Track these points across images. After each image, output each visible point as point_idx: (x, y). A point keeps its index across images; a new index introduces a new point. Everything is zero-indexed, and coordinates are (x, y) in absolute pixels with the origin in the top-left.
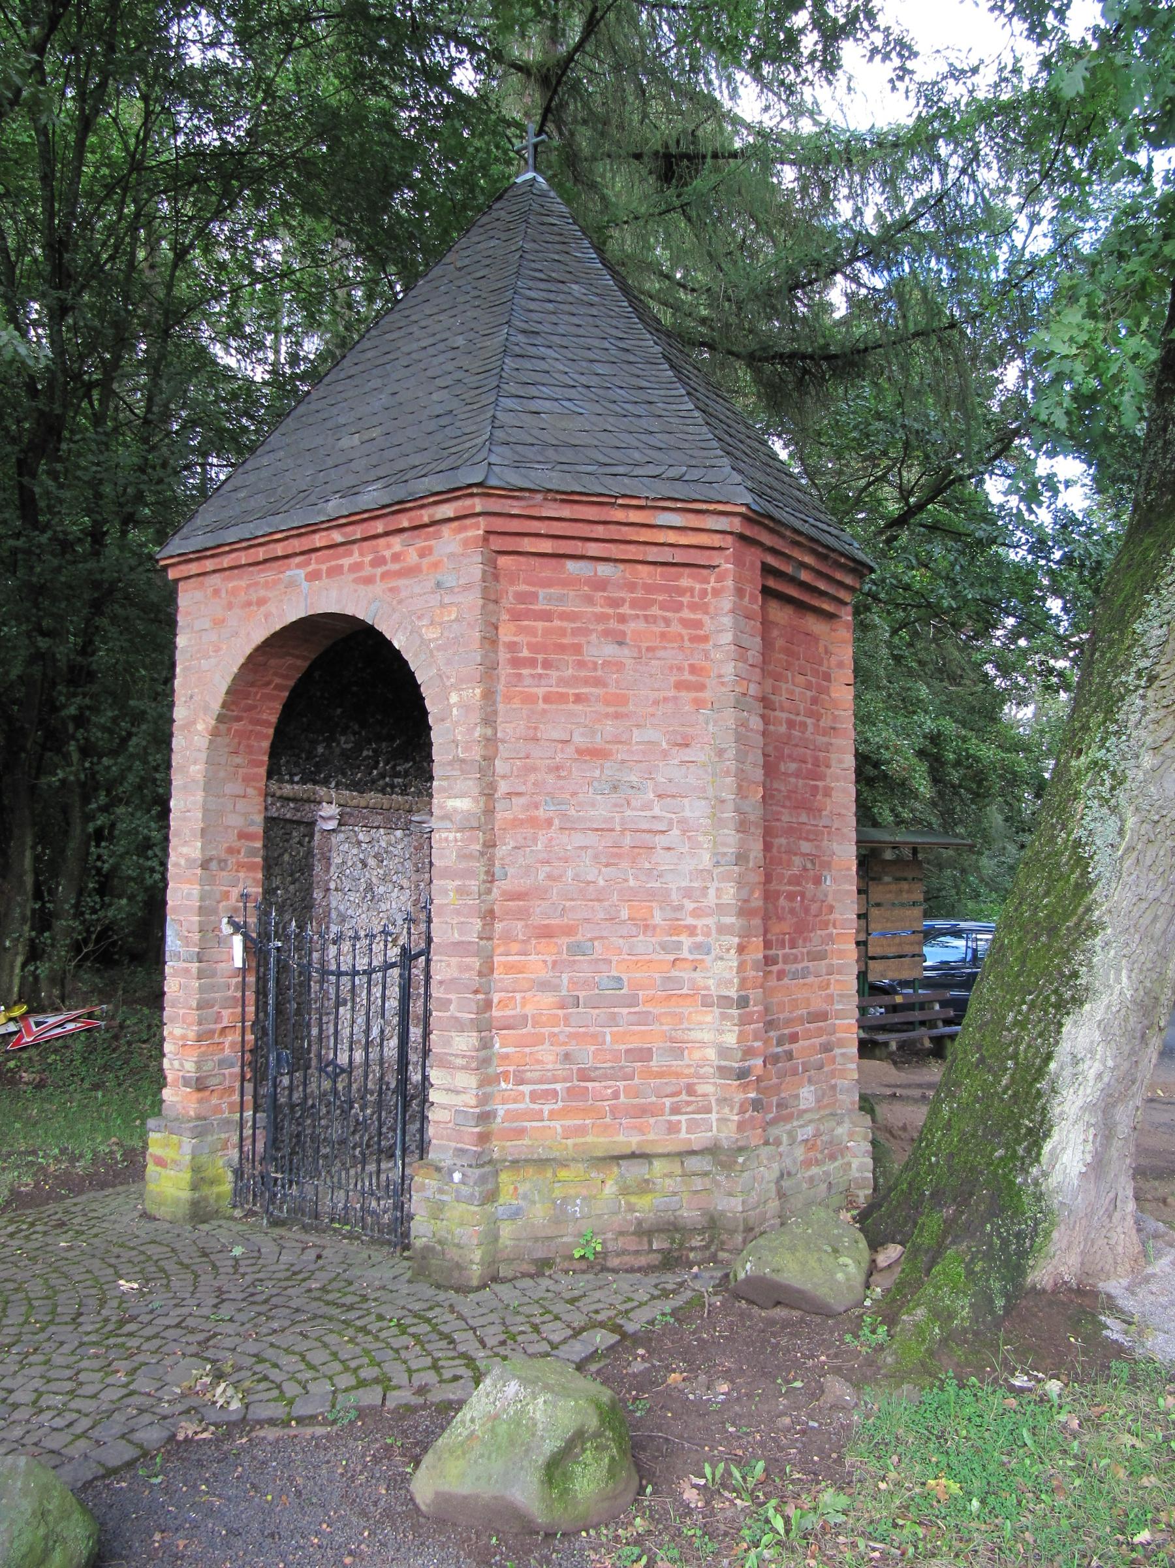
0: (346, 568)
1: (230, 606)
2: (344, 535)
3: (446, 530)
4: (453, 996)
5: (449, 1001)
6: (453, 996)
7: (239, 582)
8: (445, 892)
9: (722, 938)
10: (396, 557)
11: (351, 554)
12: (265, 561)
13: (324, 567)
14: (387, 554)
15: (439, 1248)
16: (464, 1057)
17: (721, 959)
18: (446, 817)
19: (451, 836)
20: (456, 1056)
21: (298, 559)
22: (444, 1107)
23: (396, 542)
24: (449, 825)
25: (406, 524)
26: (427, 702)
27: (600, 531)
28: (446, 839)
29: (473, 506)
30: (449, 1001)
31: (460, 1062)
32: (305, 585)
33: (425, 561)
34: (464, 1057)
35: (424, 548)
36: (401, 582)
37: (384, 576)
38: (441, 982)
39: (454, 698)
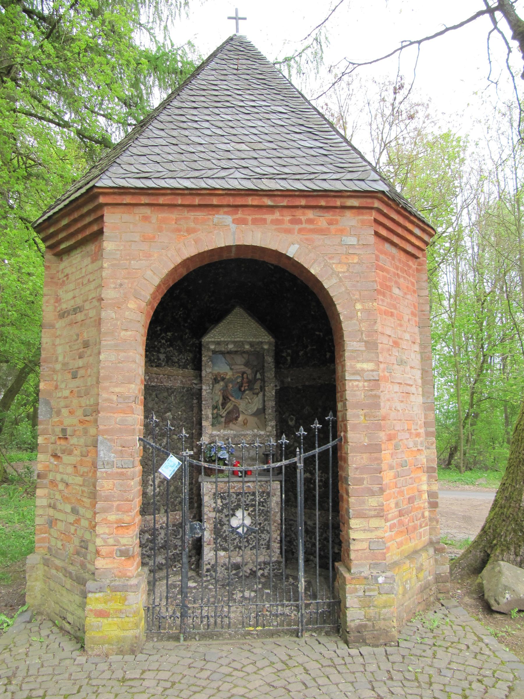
0: (268, 221)
1: (160, 229)
2: (327, 202)
3: (348, 213)
4: (365, 476)
5: (363, 479)
6: (365, 476)
7: (173, 215)
8: (358, 416)
9: (429, 438)
10: (310, 221)
11: (273, 213)
12: (200, 206)
13: (250, 218)
14: (303, 218)
15: (370, 623)
16: (375, 510)
17: (428, 448)
18: (357, 373)
19: (361, 384)
20: (370, 510)
21: (226, 209)
22: (362, 540)
23: (310, 214)
24: (358, 378)
25: (250, 203)
26: (338, 307)
27: (400, 231)
28: (357, 386)
29: (373, 203)
30: (363, 479)
31: (373, 513)
32: (233, 226)
33: (332, 227)
34: (375, 510)
35: (331, 220)
36: (316, 236)
37: (300, 231)
38: (356, 469)
39: (359, 306)
